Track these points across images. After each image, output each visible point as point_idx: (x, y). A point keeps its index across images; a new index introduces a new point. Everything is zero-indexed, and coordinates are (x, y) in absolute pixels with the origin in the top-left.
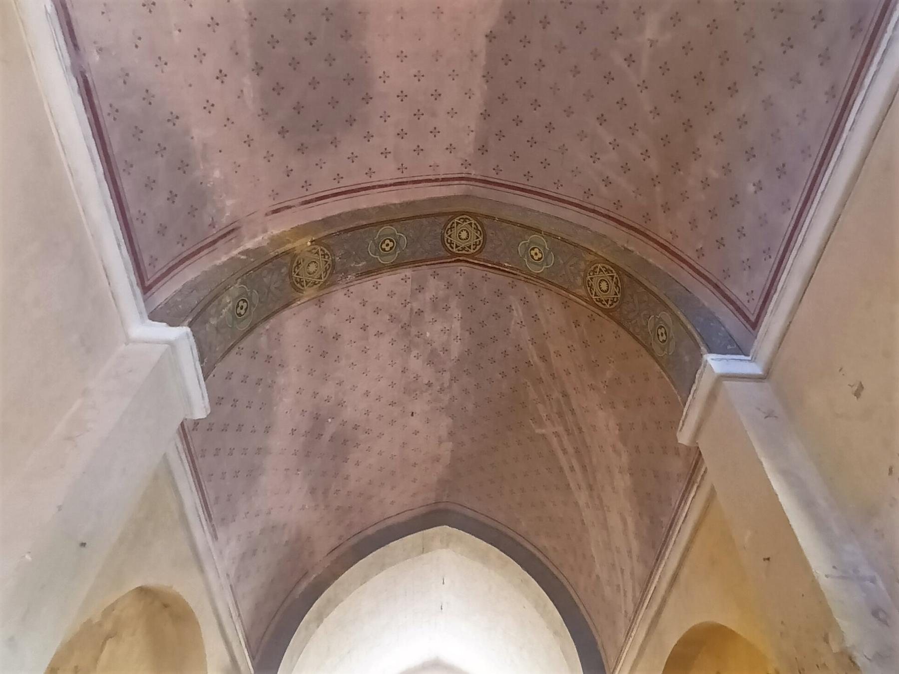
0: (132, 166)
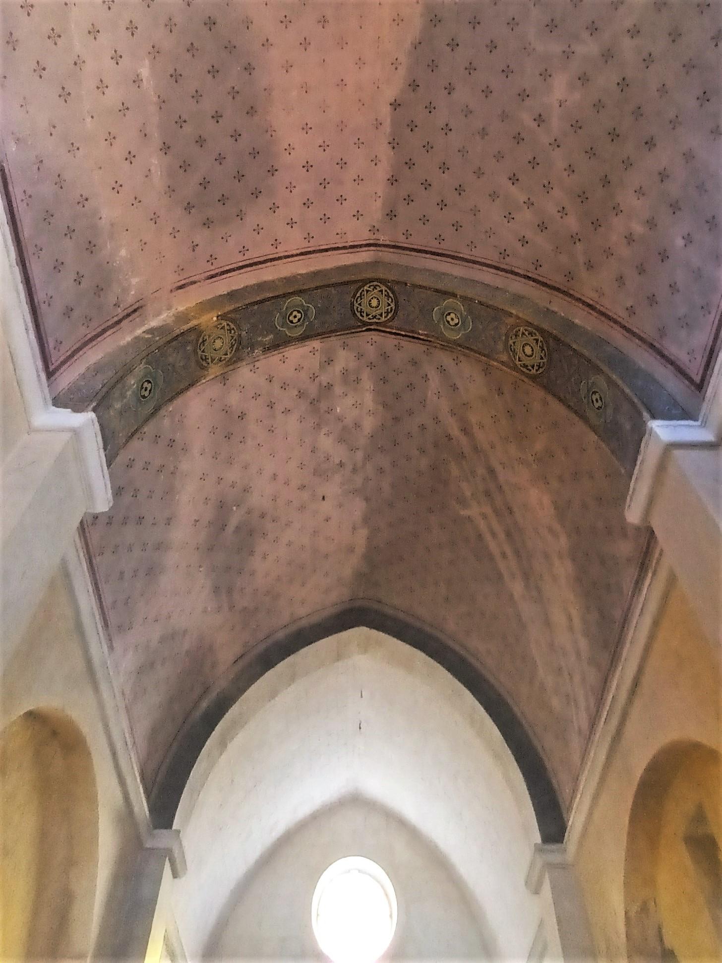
0: (41, 250)
